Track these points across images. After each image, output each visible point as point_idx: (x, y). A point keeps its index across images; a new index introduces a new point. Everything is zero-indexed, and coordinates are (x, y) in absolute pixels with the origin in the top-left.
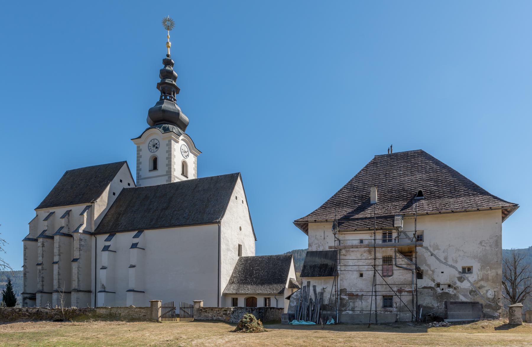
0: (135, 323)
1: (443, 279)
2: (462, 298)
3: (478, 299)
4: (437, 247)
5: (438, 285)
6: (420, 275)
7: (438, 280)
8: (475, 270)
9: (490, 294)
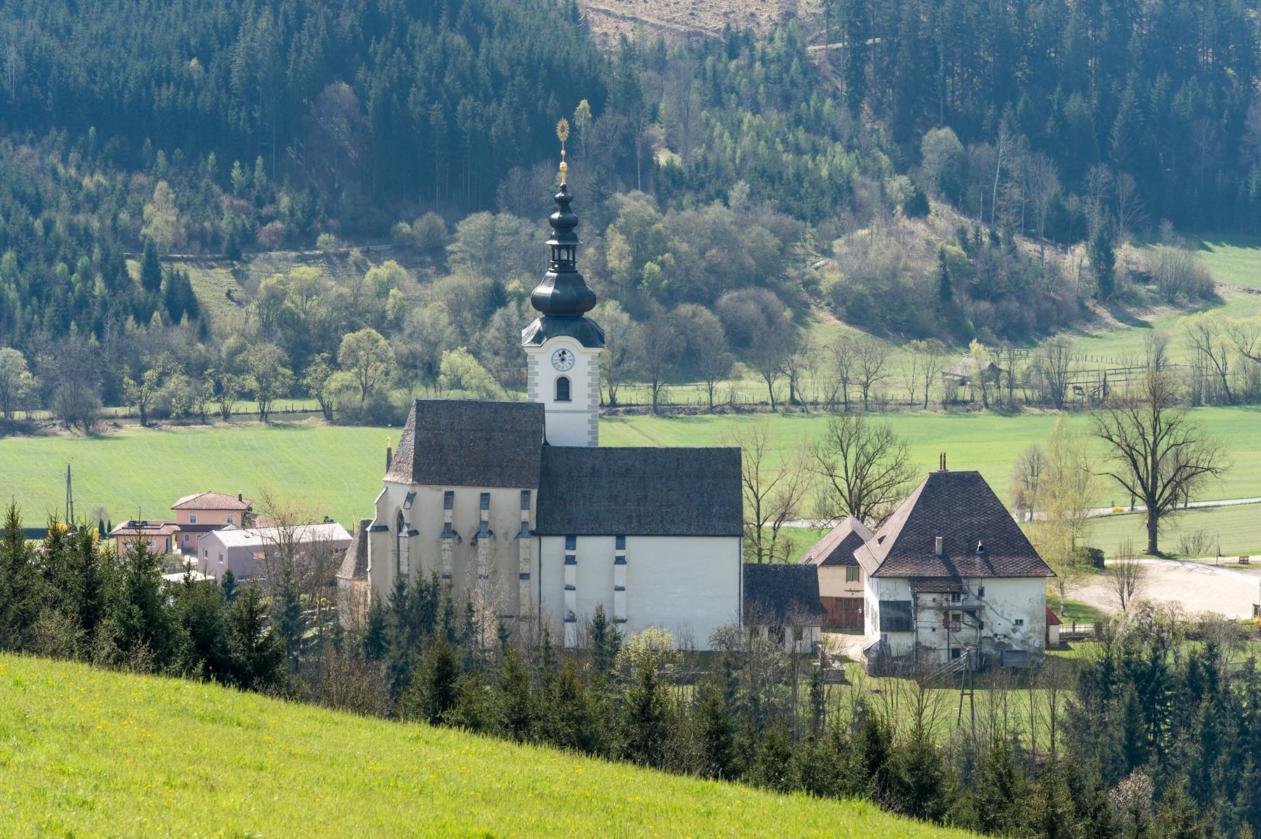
0: (337, 716)
1: (1000, 630)
2: (1015, 647)
3: (1027, 648)
4: (995, 602)
5: (996, 635)
6: (981, 627)
7: (996, 631)
8: (1025, 623)
9: (1037, 644)
